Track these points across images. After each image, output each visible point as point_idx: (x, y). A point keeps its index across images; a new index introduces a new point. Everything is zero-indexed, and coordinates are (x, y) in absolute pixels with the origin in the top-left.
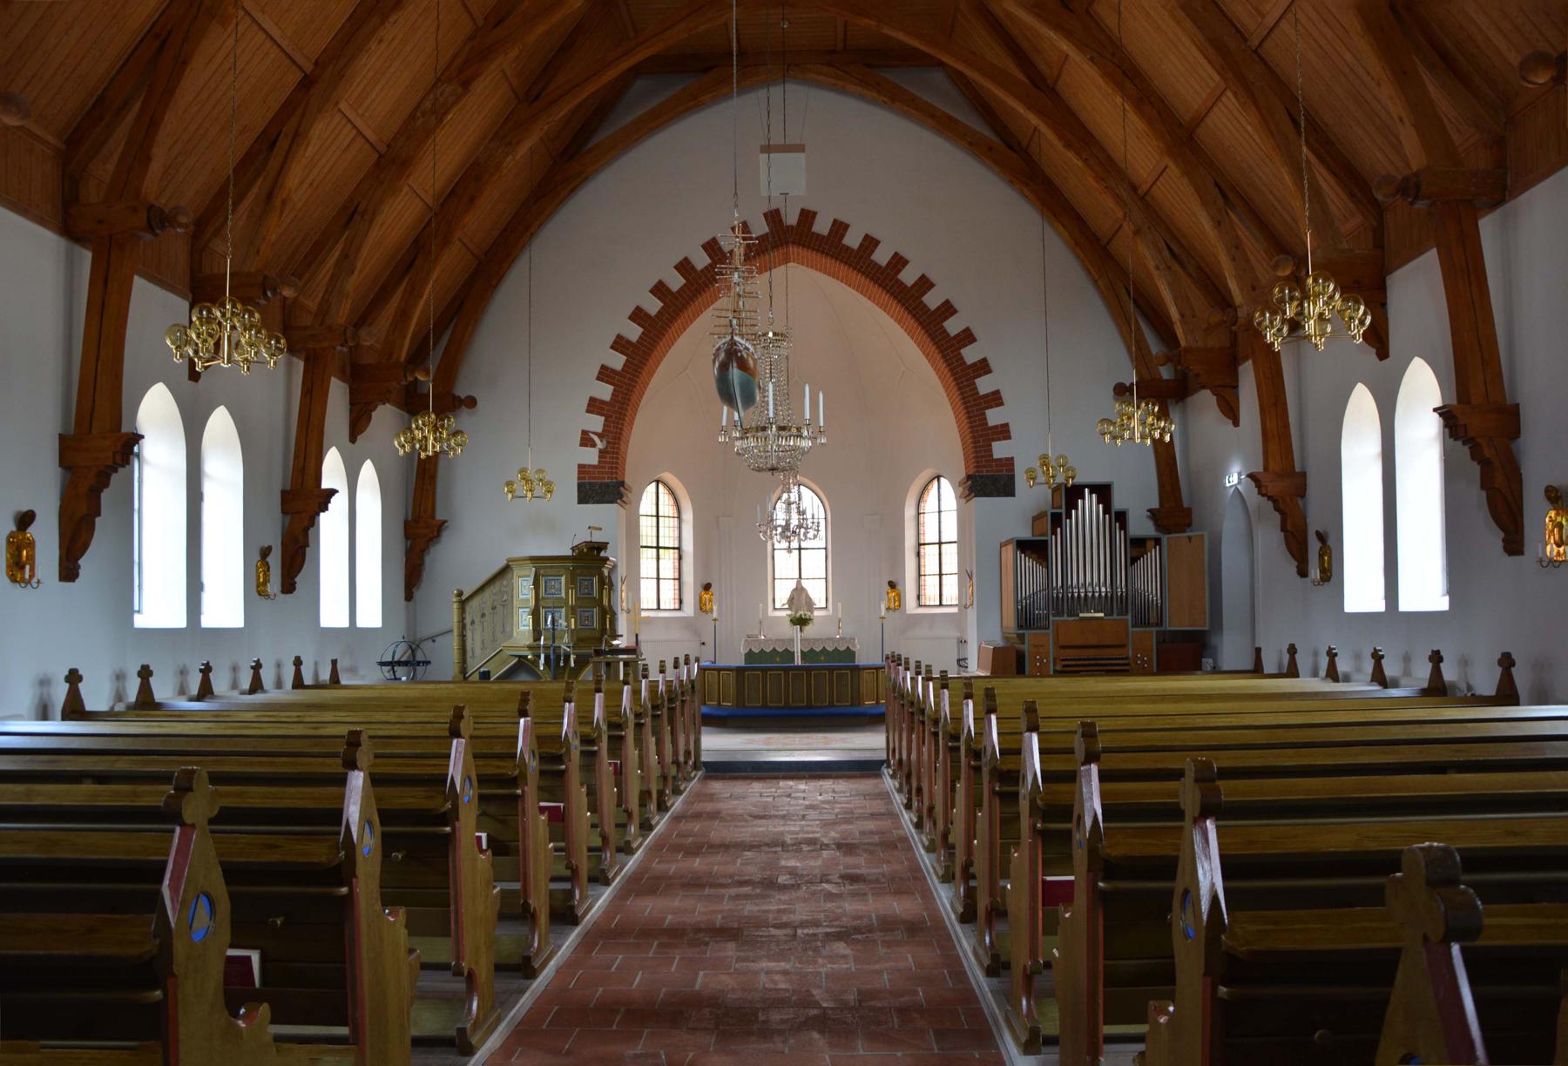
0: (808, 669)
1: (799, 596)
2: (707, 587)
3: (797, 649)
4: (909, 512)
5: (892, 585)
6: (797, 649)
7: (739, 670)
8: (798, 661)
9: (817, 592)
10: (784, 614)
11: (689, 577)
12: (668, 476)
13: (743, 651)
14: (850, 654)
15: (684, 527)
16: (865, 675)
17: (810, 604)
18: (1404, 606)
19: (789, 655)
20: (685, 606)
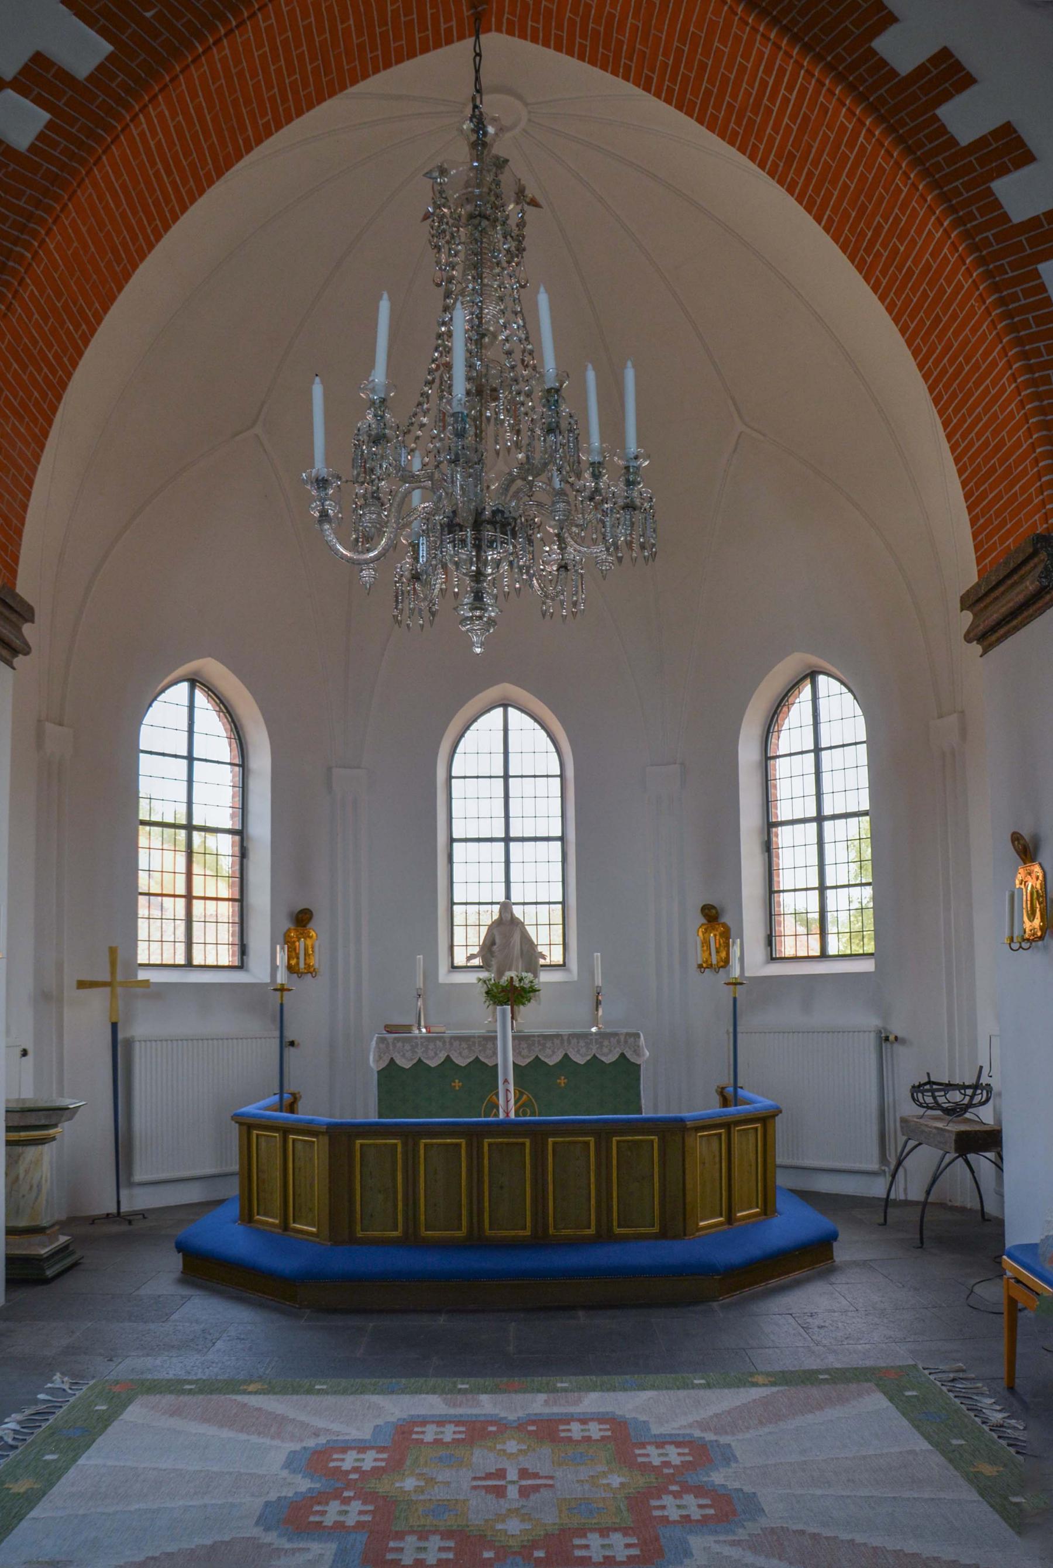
0: (538, 1133)
1: (506, 935)
2: (302, 919)
3: (506, 1059)
4: (748, 753)
5: (711, 915)
6: (506, 1059)
7: (341, 1137)
8: (507, 1104)
9: (547, 936)
10: (471, 978)
11: (261, 898)
12: (213, 668)
13: (374, 1063)
14: (626, 1071)
15: (253, 784)
16: (702, 1149)
17: (530, 953)
18: (747, 974)
19: (483, 1074)
20: (252, 960)
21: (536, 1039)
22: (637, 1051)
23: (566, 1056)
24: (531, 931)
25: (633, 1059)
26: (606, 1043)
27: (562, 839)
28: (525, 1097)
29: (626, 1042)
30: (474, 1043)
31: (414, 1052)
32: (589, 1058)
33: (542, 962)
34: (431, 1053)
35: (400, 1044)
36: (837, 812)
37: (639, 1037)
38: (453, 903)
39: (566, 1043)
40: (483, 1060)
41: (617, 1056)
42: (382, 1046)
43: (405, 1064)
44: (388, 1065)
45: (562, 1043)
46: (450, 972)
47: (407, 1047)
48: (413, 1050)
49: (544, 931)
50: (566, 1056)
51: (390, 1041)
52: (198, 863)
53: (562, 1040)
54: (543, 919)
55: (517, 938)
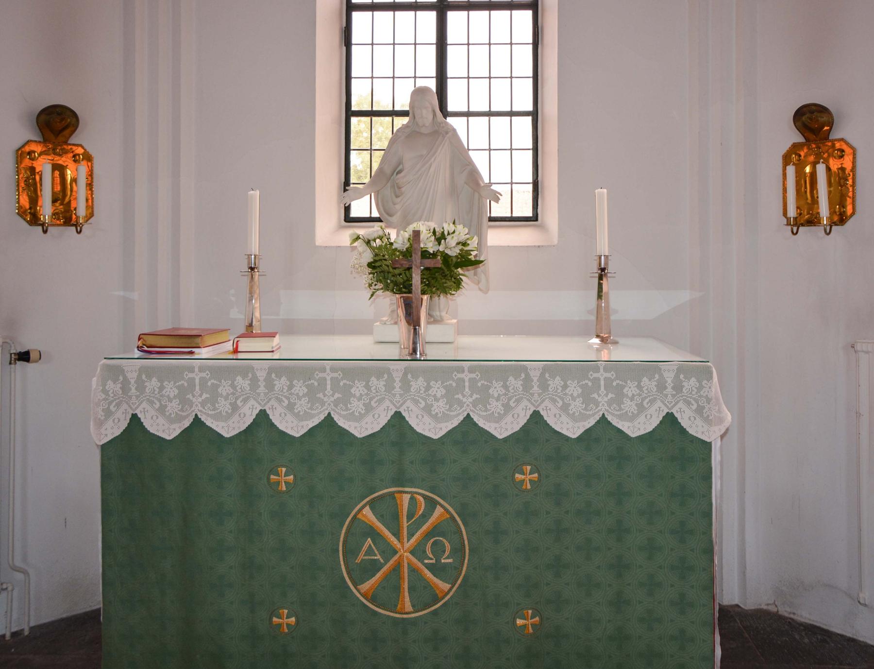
17: (471, 188)
21: (466, 376)
23: (536, 417)
24: (479, 160)
25: (695, 427)
26: (631, 389)
28: (439, 511)
29: (678, 387)
31: (185, 402)
32: (591, 422)
34: (496, 406)
36: (369, 14)
38: (534, 114)
39: (262, 389)
40: (341, 423)
41: (383, 420)
44: (525, 429)
45: (389, 387)
46: (342, 227)
49: (501, 160)
50: (536, 417)
51: (132, 376)
53: (528, 380)
54: (500, 140)
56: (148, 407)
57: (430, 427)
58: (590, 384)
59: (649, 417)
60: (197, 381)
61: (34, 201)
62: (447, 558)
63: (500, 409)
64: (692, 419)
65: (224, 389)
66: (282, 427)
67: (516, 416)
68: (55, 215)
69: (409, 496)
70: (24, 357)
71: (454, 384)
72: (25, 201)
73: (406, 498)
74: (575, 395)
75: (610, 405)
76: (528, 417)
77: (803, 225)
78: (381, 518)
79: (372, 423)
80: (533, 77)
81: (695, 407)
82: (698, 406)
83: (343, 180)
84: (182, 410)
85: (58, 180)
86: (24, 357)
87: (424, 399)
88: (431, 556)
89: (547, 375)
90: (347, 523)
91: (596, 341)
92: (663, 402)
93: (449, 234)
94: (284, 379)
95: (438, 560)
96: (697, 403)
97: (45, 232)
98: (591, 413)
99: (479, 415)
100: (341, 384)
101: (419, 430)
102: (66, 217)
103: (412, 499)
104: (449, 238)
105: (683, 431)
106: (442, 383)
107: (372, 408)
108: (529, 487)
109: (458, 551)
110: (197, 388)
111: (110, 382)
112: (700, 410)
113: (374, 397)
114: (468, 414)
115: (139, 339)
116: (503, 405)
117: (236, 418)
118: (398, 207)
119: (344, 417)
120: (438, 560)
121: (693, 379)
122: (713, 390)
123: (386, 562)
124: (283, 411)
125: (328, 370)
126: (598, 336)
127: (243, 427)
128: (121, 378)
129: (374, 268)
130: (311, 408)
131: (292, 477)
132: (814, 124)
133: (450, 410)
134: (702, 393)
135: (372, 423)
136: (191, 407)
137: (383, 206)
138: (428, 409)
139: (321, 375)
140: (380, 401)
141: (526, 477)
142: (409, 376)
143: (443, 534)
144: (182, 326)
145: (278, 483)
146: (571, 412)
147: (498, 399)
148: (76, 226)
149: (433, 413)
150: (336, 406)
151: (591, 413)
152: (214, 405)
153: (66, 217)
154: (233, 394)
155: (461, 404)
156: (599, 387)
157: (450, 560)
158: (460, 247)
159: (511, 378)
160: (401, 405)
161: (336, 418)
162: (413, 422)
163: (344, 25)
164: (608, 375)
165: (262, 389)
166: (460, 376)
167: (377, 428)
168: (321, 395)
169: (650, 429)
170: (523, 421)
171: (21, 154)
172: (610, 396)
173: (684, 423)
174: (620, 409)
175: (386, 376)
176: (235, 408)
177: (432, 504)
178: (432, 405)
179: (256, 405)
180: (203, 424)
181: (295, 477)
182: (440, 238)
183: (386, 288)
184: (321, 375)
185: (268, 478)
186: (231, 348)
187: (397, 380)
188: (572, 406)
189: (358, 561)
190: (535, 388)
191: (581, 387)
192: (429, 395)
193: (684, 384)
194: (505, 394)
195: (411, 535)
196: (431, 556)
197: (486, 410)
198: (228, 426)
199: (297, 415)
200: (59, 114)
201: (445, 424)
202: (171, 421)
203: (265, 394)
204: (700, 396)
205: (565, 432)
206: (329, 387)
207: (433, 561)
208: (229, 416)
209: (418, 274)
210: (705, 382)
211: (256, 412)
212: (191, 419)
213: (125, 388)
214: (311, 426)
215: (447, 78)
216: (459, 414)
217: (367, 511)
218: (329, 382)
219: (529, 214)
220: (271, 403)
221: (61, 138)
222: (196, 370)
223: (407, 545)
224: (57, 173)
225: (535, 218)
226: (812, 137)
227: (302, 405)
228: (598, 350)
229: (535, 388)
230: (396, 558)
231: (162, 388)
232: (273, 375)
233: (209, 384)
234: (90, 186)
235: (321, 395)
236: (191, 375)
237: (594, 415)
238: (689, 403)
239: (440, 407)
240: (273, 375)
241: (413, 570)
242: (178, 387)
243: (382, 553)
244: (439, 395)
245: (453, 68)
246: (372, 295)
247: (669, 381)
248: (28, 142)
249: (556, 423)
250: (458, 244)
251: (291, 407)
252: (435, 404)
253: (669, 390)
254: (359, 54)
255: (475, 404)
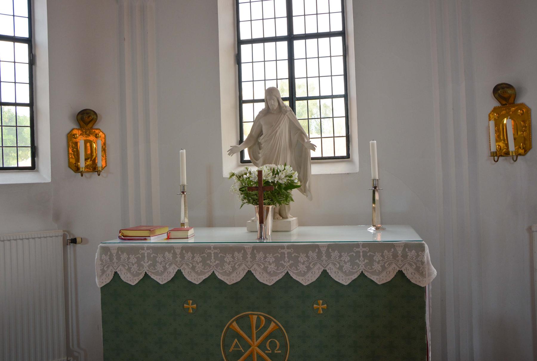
17: (300, 143)
21: (361, 249)
22: (420, 269)
23: (325, 272)
25: (414, 278)
27: (29, 41)
28: (272, 325)
29: (405, 256)
30: (209, 255)
31: (140, 266)
33: (314, 154)
34: (302, 268)
35: (124, 256)
36: (266, 36)
37: (423, 250)
38: (241, 102)
39: (178, 259)
40: (220, 277)
41: (392, 276)
42: (106, 258)
43: (132, 280)
45: (245, 257)
47: (133, 259)
48: (139, 263)
50: (325, 272)
52: (25, 117)
55: (284, 128)
56: (122, 268)
57: (195, 279)
58: (354, 255)
59: (388, 273)
60: (146, 255)
61: (78, 160)
62: (278, 350)
63: (305, 269)
64: (413, 274)
65: (160, 259)
66: (189, 279)
67: (313, 273)
68: (87, 167)
69: (256, 316)
70: (74, 241)
71: (279, 256)
72: (73, 161)
73: (255, 317)
74: (346, 261)
75: (366, 267)
76: (245, 274)
77: (501, 156)
78: (242, 328)
79: (311, 277)
80: (344, 75)
81: (414, 267)
82: (417, 266)
83: (239, 139)
84: (139, 270)
85: (89, 148)
86: (74, 241)
87: (264, 264)
88: (269, 349)
89: (330, 250)
90: (224, 330)
91: (373, 228)
92: (396, 265)
93: (280, 171)
94: (189, 253)
95: (273, 351)
96: (416, 265)
97: (82, 175)
98: (355, 271)
99: (293, 273)
100: (219, 256)
101: (261, 280)
102: (94, 168)
103: (259, 319)
104: (280, 174)
105: (409, 281)
106: (273, 255)
107: (236, 269)
108: (321, 312)
109: (284, 346)
110: (146, 258)
111: (103, 255)
112: (417, 269)
113: (236, 263)
114: (287, 272)
115: (120, 232)
116: (381, 266)
117: (166, 274)
118: (260, 155)
119: (221, 273)
120: (273, 351)
121: (414, 251)
122: (426, 257)
123: (245, 351)
124: (125, 271)
125: (212, 249)
126: (374, 226)
127: (170, 279)
128: (109, 253)
129: (243, 191)
130: (204, 269)
131: (195, 305)
132: (505, 96)
133: (277, 270)
134: (419, 259)
135: (236, 277)
136: (143, 268)
137: (253, 155)
138: (265, 269)
139: (209, 251)
140: (240, 265)
141: (320, 306)
142: (255, 251)
143: (275, 337)
144: (142, 225)
145: (188, 308)
146: (344, 270)
147: (303, 264)
148: (98, 172)
149: (268, 271)
150: (217, 268)
151: (355, 271)
152: (222, 268)
153: (94, 168)
154: (164, 261)
155: (283, 266)
156: (360, 257)
157: (280, 352)
158: (287, 178)
159: (310, 252)
160: (251, 267)
161: (217, 274)
162: (258, 276)
163: (237, 53)
164: (364, 249)
165: (178, 259)
166: (282, 251)
167: (239, 279)
168: (209, 262)
169: (389, 279)
170: (317, 276)
171: (71, 136)
172: (366, 261)
173: (409, 276)
174: (372, 269)
175: (243, 251)
176: (165, 269)
177: (269, 321)
178: (268, 267)
179: (176, 267)
180: (149, 277)
181: (197, 305)
182: (275, 173)
183: (249, 202)
184: (209, 251)
185: (183, 305)
186: (166, 237)
187: (249, 253)
188: (345, 267)
189: (231, 351)
190: (324, 257)
191: (350, 256)
192: (266, 262)
193: (408, 254)
194: (307, 261)
195: (258, 338)
196: (269, 349)
197: (297, 270)
198: (162, 279)
199: (197, 273)
200: (87, 114)
201: (275, 277)
202: (134, 275)
203: (117, 263)
204: (418, 261)
205: (341, 282)
206: (213, 257)
207: (270, 352)
208: (162, 273)
209: (265, 194)
210: (420, 252)
211: (176, 271)
212: (143, 274)
213: (111, 259)
214: (204, 278)
215: (295, 78)
216: (282, 272)
217: (235, 324)
218: (213, 255)
219: (344, 154)
220: (119, 268)
221: (90, 125)
222: (145, 249)
223: (256, 343)
224: (88, 144)
225: (348, 156)
226: (504, 102)
227: (199, 267)
228: (374, 235)
229: (324, 257)
230: (250, 349)
231: (129, 258)
232: (184, 251)
233: (152, 256)
234: (104, 150)
235: (209, 262)
236: (143, 252)
237: (357, 272)
238: (411, 265)
239: (272, 268)
240: (184, 251)
241: (259, 356)
242: (137, 258)
243: (243, 347)
244: (271, 261)
245: (299, 72)
246: (242, 205)
247: (400, 252)
248: (73, 129)
249: (260, 278)
250: (286, 176)
251: (193, 268)
252: (270, 267)
253: (400, 258)
254: (246, 69)
255: (291, 266)
